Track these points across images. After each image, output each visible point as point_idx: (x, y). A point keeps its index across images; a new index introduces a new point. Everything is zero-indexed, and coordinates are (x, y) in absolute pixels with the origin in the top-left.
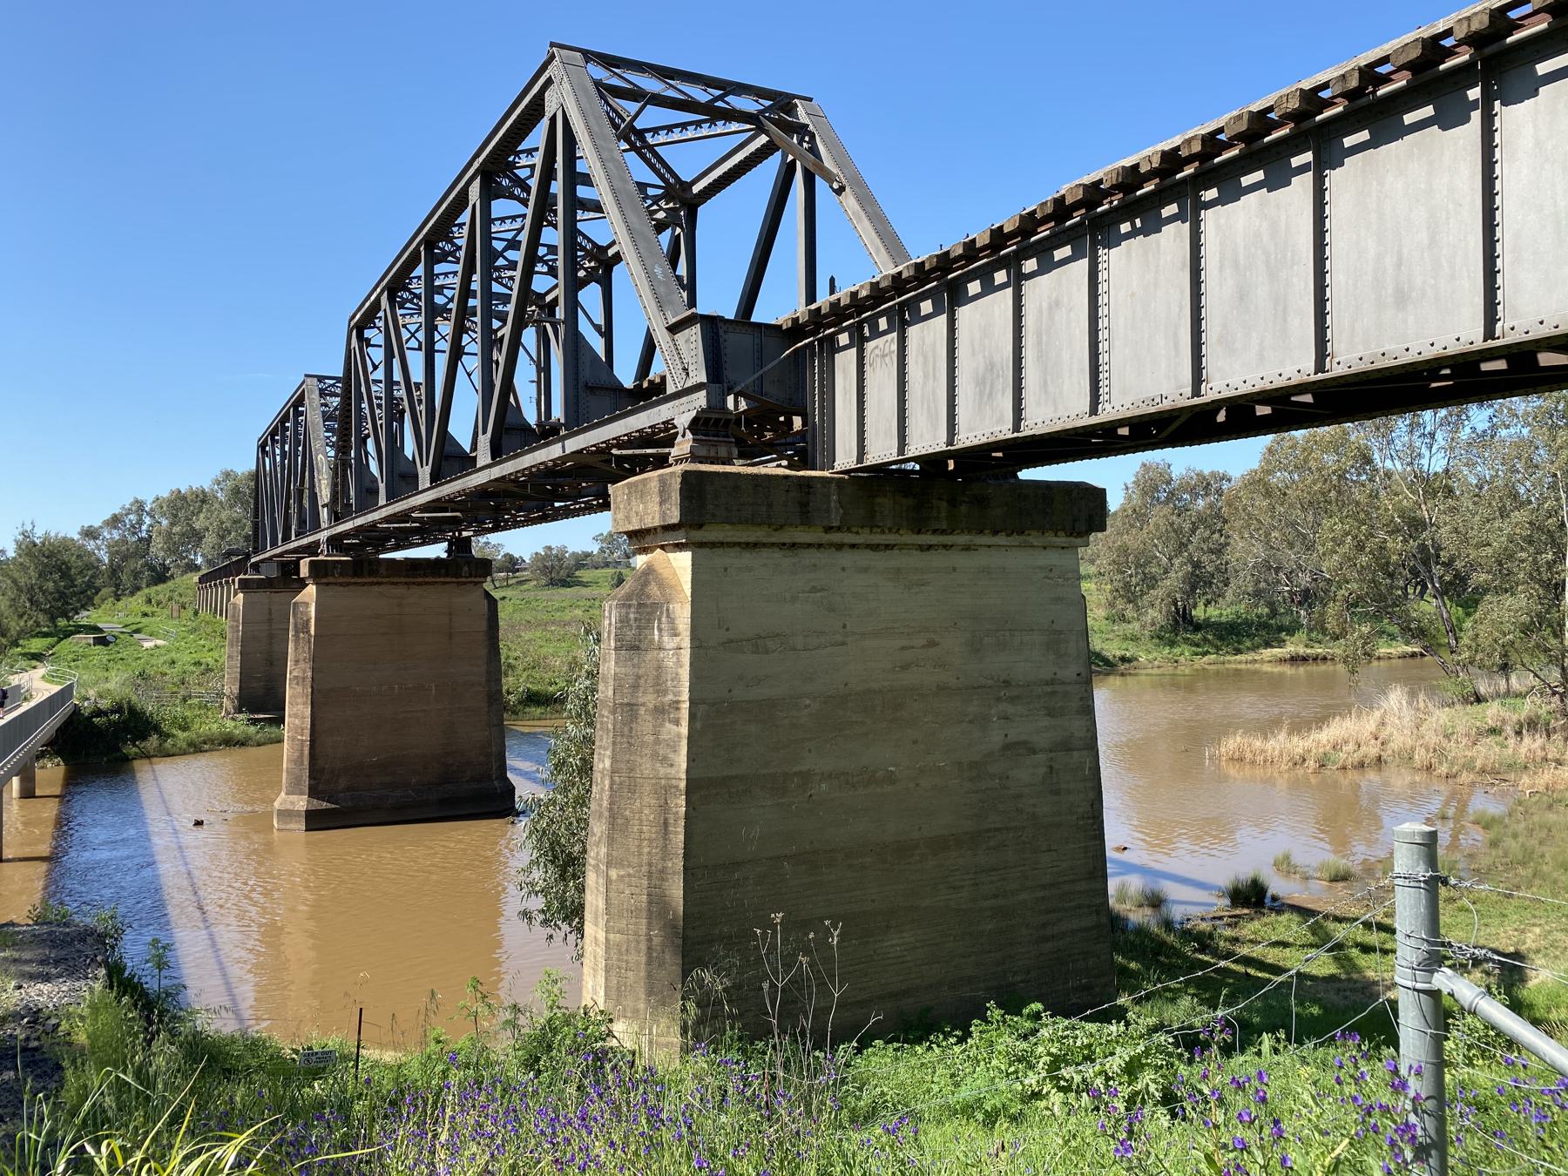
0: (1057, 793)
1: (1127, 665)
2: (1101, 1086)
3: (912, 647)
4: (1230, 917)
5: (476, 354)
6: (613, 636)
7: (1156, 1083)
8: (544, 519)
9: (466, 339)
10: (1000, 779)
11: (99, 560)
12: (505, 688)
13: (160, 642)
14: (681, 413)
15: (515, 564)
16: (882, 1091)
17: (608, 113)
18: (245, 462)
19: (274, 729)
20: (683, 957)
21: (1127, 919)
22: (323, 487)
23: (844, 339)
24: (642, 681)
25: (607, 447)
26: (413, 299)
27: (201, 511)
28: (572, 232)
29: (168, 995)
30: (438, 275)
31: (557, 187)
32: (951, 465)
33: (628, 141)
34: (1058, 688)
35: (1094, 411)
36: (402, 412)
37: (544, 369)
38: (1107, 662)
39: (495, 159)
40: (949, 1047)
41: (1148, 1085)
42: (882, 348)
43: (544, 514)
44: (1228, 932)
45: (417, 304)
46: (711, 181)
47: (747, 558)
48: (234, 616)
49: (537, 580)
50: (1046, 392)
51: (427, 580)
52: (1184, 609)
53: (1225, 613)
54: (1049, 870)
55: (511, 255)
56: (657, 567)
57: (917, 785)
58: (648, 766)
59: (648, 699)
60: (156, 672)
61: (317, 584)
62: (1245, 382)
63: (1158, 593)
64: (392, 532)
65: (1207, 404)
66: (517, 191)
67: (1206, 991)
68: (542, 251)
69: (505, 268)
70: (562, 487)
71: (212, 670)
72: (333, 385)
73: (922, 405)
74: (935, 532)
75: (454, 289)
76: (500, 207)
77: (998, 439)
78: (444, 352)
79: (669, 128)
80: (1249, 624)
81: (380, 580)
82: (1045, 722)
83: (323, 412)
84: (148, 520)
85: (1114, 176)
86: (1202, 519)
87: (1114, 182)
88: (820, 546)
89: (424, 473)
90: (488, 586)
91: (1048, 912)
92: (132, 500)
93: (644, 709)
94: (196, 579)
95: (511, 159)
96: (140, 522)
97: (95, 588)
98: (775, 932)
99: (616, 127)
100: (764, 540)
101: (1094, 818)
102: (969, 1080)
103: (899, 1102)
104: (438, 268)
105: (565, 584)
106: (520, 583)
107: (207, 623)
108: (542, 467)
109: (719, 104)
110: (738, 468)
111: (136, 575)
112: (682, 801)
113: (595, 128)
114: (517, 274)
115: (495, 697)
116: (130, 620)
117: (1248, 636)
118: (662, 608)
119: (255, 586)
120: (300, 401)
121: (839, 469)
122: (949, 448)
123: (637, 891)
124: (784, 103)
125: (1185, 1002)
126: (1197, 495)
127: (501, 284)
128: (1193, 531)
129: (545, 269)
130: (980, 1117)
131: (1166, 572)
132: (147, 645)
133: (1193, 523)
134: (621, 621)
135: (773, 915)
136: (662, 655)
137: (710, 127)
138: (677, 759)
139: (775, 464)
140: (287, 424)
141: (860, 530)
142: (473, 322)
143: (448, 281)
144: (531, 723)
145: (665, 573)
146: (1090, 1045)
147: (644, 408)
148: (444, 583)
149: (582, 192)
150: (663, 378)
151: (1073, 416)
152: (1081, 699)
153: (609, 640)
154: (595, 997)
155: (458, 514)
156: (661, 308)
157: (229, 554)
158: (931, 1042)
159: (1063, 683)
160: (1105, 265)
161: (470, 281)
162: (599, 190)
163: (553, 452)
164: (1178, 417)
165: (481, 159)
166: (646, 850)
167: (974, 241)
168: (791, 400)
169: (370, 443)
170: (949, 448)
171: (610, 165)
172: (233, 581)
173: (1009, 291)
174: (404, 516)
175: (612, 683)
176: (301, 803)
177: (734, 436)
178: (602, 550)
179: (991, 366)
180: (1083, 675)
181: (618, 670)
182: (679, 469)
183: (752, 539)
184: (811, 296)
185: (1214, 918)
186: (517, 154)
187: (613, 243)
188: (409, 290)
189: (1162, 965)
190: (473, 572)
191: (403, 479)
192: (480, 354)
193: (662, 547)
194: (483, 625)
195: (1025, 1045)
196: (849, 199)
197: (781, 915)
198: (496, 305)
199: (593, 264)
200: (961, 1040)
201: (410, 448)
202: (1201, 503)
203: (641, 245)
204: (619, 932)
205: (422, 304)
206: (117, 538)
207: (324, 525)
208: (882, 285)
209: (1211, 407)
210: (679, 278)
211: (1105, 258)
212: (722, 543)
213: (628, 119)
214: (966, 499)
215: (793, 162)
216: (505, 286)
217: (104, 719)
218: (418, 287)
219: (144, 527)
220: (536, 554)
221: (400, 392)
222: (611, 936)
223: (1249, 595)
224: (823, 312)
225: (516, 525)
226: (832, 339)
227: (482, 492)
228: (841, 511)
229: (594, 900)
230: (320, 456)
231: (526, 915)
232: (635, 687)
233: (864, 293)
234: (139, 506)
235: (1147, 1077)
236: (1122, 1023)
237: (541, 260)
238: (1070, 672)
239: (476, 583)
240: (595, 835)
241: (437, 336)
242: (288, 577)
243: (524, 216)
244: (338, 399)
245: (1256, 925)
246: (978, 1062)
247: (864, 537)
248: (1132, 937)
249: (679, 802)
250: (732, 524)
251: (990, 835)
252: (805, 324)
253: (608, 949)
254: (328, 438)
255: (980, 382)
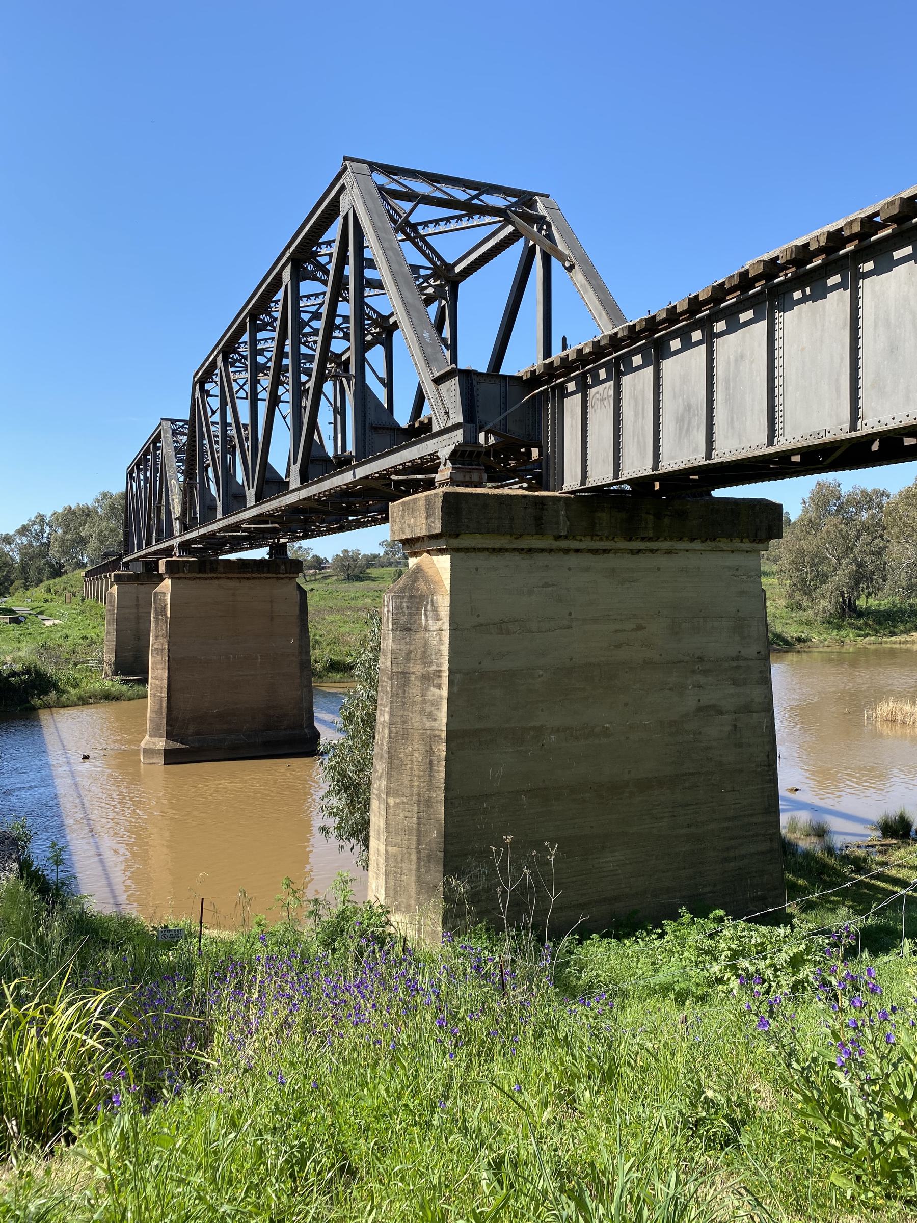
0: (740, 745)
1: (802, 645)
2: (771, 976)
3: (624, 631)
4: (881, 845)
5: (288, 402)
6: (390, 620)
7: (814, 974)
8: (341, 529)
9: (281, 390)
10: (694, 734)
11: (13, 560)
12: (313, 659)
13: (57, 621)
14: (443, 447)
15: (321, 563)
16: (597, 973)
17: (388, 211)
18: (118, 486)
19: (141, 688)
20: (445, 866)
21: (797, 846)
22: (175, 505)
23: (571, 386)
24: (413, 655)
25: (387, 474)
26: (241, 359)
27: (85, 523)
28: (360, 304)
29: (63, 884)
30: (260, 341)
31: (349, 270)
32: (657, 486)
33: (404, 233)
34: (742, 663)
35: (770, 443)
36: (234, 447)
37: (340, 412)
38: (786, 641)
39: (302, 249)
40: (652, 941)
41: (808, 976)
42: (602, 393)
43: (341, 525)
44: (879, 858)
45: (244, 364)
46: (469, 262)
47: (495, 561)
48: (110, 602)
49: (337, 575)
50: (733, 428)
51: (254, 575)
52: (850, 600)
53: (883, 603)
54: (733, 806)
55: (315, 324)
56: (424, 567)
57: (627, 738)
58: (417, 720)
59: (418, 669)
60: (54, 644)
61: (171, 578)
62: (893, 419)
63: (829, 586)
64: (227, 539)
65: (862, 437)
66: (320, 274)
67: (860, 903)
68: (338, 321)
69: (310, 334)
70: (354, 504)
71: (95, 643)
72: (182, 427)
73: (633, 439)
74: (643, 539)
75: (272, 351)
76: (306, 287)
77: (693, 465)
78: (265, 400)
79: (437, 222)
80: (902, 612)
81: (219, 575)
82: (732, 690)
83: (175, 447)
84: (47, 530)
85: (789, 253)
86: (865, 528)
87: (789, 258)
88: (551, 551)
89: (251, 494)
90: (300, 580)
91: (731, 839)
92: (36, 514)
93: (414, 676)
94: (83, 574)
95: (314, 249)
96: (42, 531)
97: (10, 580)
98: (506, 849)
99: (395, 221)
100: (507, 546)
101: (769, 766)
102: (664, 968)
103: (610, 982)
104: (260, 335)
105: (359, 579)
106: (325, 578)
107: (92, 607)
108: (338, 489)
109: (476, 201)
110: (489, 490)
111: (40, 571)
112: (443, 747)
113: (379, 224)
114: (319, 339)
115: (305, 665)
116: (36, 604)
117: (902, 622)
118: (428, 599)
119: (126, 580)
120: (157, 439)
121: (567, 490)
122: (654, 472)
123: (410, 815)
124: (526, 199)
125: (843, 911)
126: (862, 508)
127: (308, 347)
128: (858, 537)
129: (341, 335)
130: (672, 996)
131: (835, 570)
132: (48, 623)
133: (858, 531)
134: (396, 609)
135: (505, 837)
136: (427, 635)
137: (468, 220)
138: (439, 715)
139: (517, 486)
140: (148, 457)
141: (583, 539)
142: (287, 377)
143: (267, 345)
144: (332, 685)
145: (430, 572)
146: (763, 943)
147: (415, 444)
148: (267, 578)
149: (368, 273)
150: (430, 419)
151: (754, 447)
152: (761, 672)
153: (388, 623)
154: (378, 895)
155: (276, 525)
156: (428, 364)
157: (107, 555)
158: (637, 937)
159: (746, 659)
160: (781, 326)
161: (283, 345)
162: (381, 273)
163: (346, 478)
164: (839, 447)
165: (291, 250)
166: (416, 784)
167: (675, 307)
168: (529, 435)
169: (210, 470)
170: (654, 472)
171: (390, 253)
172: (110, 575)
173: (703, 347)
174: (236, 527)
175: (390, 656)
176: (161, 744)
177: (484, 464)
178: (386, 553)
179: (688, 407)
180: (763, 653)
181: (394, 646)
182: (440, 491)
183: (497, 546)
184: (547, 352)
185: (868, 846)
186: (319, 245)
187: (392, 315)
188: (238, 353)
189: (825, 882)
190: (289, 571)
191: (234, 500)
192: (291, 402)
193: (428, 552)
194: (296, 611)
195: (710, 942)
196: (578, 276)
197: (511, 837)
198: (304, 363)
199: (378, 330)
200: (661, 936)
201: (240, 477)
202: (864, 515)
203: (413, 314)
204: (395, 846)
205: (248, 363)
206: (26, 543)
207: (176, 534)
208: (602, 343)
209: (865, 440)
210: (444, 341)
211: (781, 320)
212: (474, 549)
213: (404, 216)
214: (669, 513)
215: (534, 246)
216: (311, 348)
217: (18, 679)
218: (245, 350)
219: (45, 535)
220: (337, 555)
221: (232, 432)
222: (390, 849)
223: (903, 588)
224: (555, 365)
225: (320, 534)
226: (562, 386)
227: (294, 509)
228: (568, 523)
229: (377, 821)
230: (173, 481)
231: (324, 829)
232: (407, 659)
233: (587, 350)
234: (41, 518)
235: (808, 970)
236: (788, 927)
237: (338, 327)
238: (751, 651)
239: (291, 578)
240: (377, 771)
241: (259, 389)
242: (150, 574)
243: (324, 293)
244: (186, 437)
245: (903, 852)
246: (673, 953)
247: (587, 544)
248: (800, 860)
249: (441, 747)
250: (481, 533)
251: (685, 778)
252: (541, 375)
253: (387, 858)
254: (179, 467)
255: (680, 420)
